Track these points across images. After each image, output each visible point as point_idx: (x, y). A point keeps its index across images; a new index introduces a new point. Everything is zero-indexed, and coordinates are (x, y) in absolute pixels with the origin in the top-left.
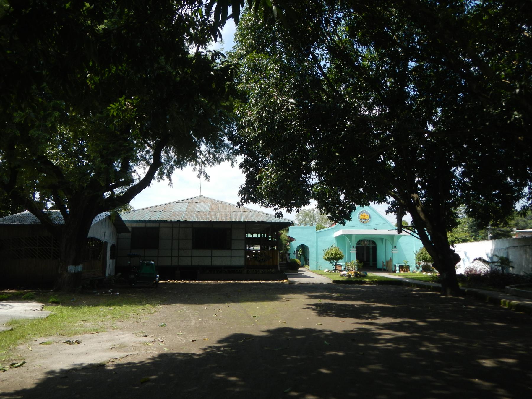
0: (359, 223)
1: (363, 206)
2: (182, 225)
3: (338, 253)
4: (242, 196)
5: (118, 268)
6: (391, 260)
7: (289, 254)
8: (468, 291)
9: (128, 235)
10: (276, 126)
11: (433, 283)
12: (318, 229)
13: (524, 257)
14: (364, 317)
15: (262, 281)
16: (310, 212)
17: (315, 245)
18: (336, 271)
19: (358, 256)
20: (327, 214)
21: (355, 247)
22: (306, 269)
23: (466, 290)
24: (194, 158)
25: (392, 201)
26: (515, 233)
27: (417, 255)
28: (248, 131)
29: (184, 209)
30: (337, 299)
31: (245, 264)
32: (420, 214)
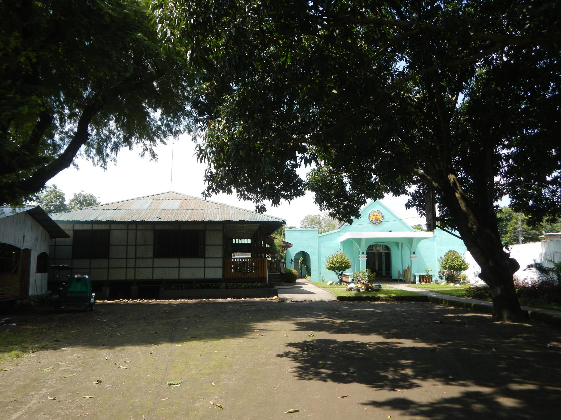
0: (370, 225)
1: (375, 200)
2: (140, 227)
3: (344, 260)
4: (210, 184)
5: (52, 285)
6: (409, 268)
7: (284, 263)
8: (533, 313)
9: (69, 241)
12: (321, 233)
14: (386, 378)
15: (244, 298)
16: (316, 218)
18: (342, 283)
19: (369, 265)
20: (329, 209)
21: (365, 253)
22: (307, 281)
23: (529, 312)
25: (413, 192)
26: (543, 236)
27: (442, 262)
28: (162, 30)
29: (146, 206)
30: (340, 330)
31: (223, 275)
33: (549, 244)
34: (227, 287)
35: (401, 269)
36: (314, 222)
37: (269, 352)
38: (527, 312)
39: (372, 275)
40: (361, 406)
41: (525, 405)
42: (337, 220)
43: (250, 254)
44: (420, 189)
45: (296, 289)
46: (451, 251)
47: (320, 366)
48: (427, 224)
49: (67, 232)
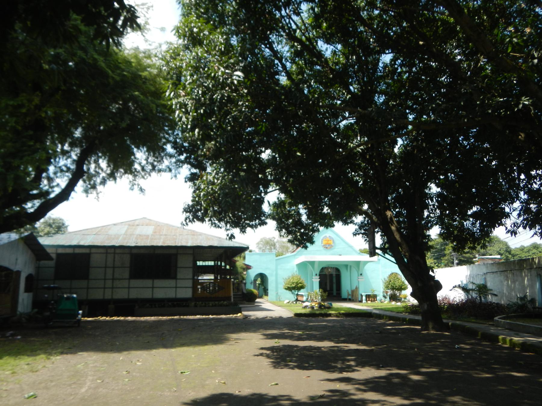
0: (322, 248)
1: (327, 228)
2: (118, 251)
3: (300, 281)
5: (35, 304)
6: (357, 288)
7: (245, 284)
9: (52, 263)
10: (217, 107)
11: (407, 314)
13: (505, 283)
14: (336, 367)
15: (212, 315)
17: (275, 272)
19: (322, 285)
21: (318, 275)
22: (264, 300)
23: (450, 324)
24: (129, 169)
26: (477, 259)
28: (178, 115)
29: (123, 232)
32: (395, 234)
33: (472, 267)
34: (196, 306)
35: (350, 288)
36: (269, 244)
37: (247, 354)
38: (448, 323)
39: (324, 294)
40: (320, 381)
41: (426, 379)
42: (295, 247)
43: (213, 275)
44: (365, 220)
45: (257, 307)
46: (393, 273)
47: (288, 361)
48: (369, 252)
49: (52, 255)
